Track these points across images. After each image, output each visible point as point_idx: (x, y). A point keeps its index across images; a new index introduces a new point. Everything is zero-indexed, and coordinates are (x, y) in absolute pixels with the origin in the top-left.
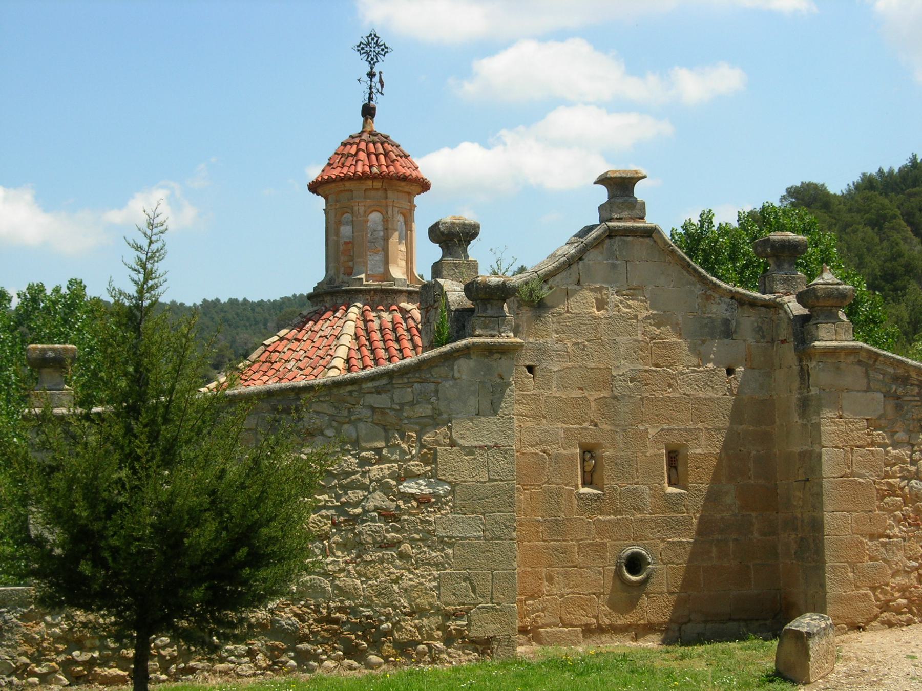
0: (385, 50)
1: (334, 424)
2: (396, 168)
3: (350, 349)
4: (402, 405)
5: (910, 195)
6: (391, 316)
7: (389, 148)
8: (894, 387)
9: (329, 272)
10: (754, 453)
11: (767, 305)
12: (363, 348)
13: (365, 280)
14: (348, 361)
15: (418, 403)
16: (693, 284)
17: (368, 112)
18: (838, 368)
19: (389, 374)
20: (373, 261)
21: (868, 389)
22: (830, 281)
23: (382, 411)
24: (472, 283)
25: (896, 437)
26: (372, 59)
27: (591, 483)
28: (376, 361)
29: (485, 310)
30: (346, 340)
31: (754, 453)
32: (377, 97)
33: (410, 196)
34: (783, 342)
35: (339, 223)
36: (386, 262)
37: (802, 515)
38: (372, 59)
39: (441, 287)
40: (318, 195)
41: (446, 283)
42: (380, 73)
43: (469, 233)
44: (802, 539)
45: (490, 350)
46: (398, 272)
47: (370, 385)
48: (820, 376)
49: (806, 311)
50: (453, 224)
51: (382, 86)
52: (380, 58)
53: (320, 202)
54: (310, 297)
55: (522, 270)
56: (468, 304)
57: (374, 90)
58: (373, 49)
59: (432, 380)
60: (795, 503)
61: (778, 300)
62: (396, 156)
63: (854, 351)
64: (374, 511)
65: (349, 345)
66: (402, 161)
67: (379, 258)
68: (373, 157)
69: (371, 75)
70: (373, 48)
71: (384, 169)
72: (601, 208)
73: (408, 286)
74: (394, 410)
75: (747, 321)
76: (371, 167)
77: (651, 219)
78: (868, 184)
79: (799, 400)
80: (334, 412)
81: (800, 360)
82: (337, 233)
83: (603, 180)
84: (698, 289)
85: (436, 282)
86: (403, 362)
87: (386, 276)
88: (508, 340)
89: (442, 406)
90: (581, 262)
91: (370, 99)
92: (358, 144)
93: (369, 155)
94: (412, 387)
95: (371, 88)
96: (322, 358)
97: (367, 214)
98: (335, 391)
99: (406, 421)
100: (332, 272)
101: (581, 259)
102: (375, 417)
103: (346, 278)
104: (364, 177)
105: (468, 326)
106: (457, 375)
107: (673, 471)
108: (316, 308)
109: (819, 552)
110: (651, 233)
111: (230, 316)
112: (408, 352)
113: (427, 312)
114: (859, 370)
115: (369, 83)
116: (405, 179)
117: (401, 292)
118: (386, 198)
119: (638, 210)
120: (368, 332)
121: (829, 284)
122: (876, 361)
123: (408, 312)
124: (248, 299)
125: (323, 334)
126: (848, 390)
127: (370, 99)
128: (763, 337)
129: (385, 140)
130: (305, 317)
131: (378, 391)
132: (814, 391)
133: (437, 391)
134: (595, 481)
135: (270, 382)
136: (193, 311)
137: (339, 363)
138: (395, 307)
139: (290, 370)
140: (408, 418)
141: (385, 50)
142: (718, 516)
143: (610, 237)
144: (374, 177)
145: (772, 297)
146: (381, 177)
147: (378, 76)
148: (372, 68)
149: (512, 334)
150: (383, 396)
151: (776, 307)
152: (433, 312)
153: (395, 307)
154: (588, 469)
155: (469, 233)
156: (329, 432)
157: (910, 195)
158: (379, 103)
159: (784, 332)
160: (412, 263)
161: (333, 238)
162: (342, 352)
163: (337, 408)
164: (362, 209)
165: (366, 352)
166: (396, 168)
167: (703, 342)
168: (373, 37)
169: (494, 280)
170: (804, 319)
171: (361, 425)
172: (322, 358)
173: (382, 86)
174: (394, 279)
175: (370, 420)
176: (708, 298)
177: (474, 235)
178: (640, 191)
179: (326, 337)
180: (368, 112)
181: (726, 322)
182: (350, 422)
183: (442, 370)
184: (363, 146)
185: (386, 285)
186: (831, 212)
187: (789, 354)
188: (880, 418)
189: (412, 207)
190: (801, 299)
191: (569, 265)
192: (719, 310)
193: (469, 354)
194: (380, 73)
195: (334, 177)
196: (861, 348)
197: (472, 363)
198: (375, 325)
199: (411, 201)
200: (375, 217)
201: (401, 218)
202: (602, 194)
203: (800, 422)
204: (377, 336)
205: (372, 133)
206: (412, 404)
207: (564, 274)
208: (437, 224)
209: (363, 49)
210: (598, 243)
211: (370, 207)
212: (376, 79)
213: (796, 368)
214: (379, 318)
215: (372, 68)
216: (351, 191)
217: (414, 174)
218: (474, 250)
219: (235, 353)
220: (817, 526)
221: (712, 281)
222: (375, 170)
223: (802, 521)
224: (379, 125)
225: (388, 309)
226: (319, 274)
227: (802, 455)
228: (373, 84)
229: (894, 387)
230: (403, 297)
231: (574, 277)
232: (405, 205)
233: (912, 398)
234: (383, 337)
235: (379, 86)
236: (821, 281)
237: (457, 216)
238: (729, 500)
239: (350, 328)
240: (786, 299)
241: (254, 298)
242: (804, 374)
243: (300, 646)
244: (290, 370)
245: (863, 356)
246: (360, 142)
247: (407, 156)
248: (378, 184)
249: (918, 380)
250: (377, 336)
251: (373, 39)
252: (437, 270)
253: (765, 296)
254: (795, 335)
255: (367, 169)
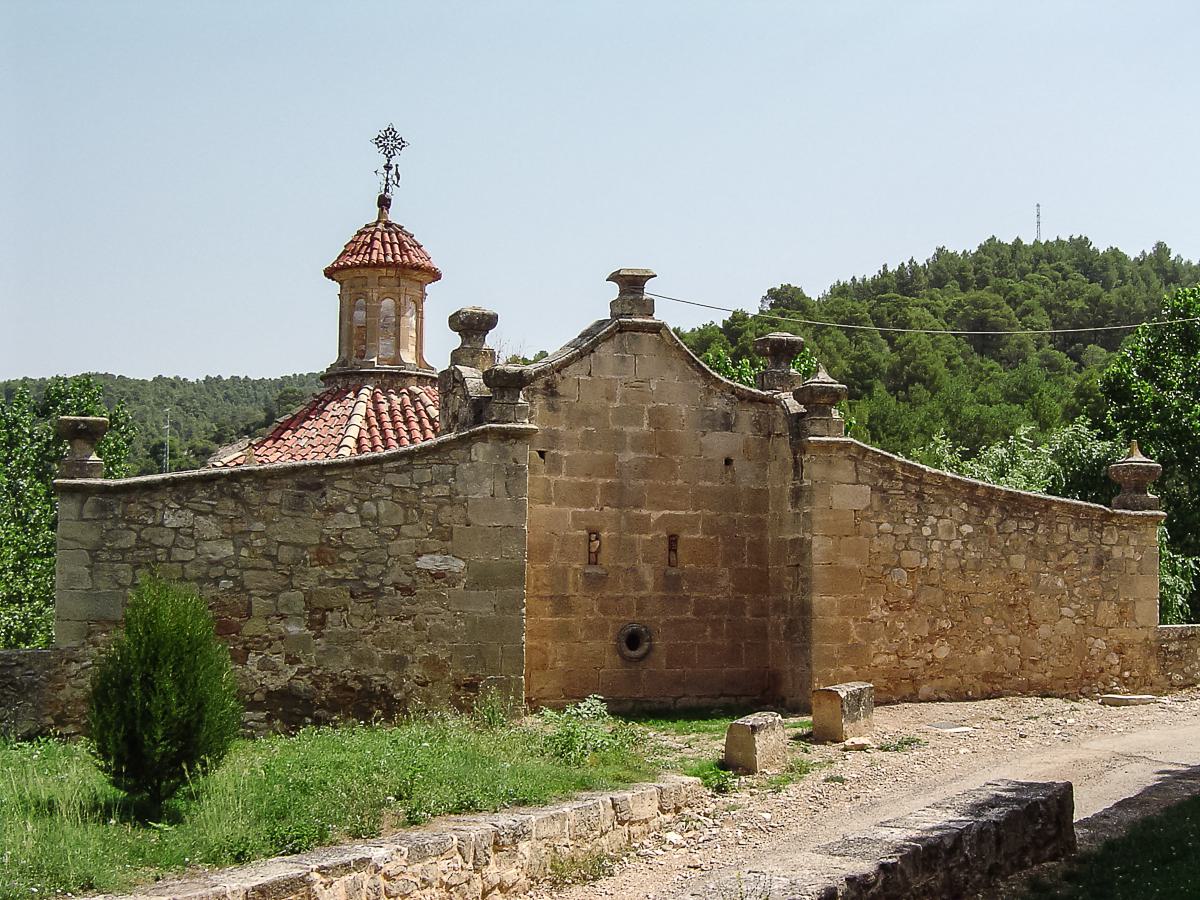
0: (402, 144)
1: (356, 501)
2: (409, 258)
3: (361, 429)
4: (421, 485)
5: (881, 300)
6: (400, 399)
7: (404, 238)
8: (881, 481)
9: (342, 355)
10: (748, 539)
11: (764, 400)
12: (374, 428)
13: (376, 362)
14: (358, 440)
15: (437, 483)
16: (697, 378)
17: (384, 203)
18: (830, 462)
19: (409, 455)
20: (384, 346)
21: (857, 483)
22: (825, 381)
23: (402, 490)
24: (490, 371)
25: (881, 527)
26: (389, 152)
27: (596, 564)
28: (412, 441)
29: (502, 397)
30: (357, 420)
31: (748, 539)
32: (393, 189)
33: (422, 285)
34: (778, 435)
35: (353, 308)
36: (398, 347)
37: (792, 599)
38: (389, 152)
39: (460, 373)
40: (333, 280)
41: (465, 371)
42: (397, 165)
43: (487, 322)
44: (791, 621)
45: (507, 435)
46: (408, 356)
47: (391, 465)
48: (814, 470)
49: (801, 409)
50: (473, 313)
51: (398, 178)
52: (397, 151)
53: (335, 287)
54: (324, 378)
55: (543, 354)
56: (486, 391)
57: (390, 182)
58: (390, 143)
59: (451, 462)
60: (786, 587)
61: (775, 396)
62: (410, 246)
63: (846, 446)
64: (391, 585)
65: (360, 425)
66: (416, 251)
67: (390, 343)
68: (388, 246)
69: (388, 167)
70: (390, 142)
71: (398, 258)
72: (613, 304)
73: (417, 370)
74: (415, 489)
75: (747, 415)
76: (385, 255)
77: (659, 316)
78: (840, 291)
79: (792, 490)
80: (357, 490)
81: (795, 454)
82: (351, 318)
83: (615, 277)
84: (700, 384)
85: (455, 368)
86: (424, 444)
87: (397, 360)
88: (523, 426)
89: (459, 487)
90: (592, 354)
91: (386, 190)
92: (373, 233)
93: (384, 244)
94: (430, 468)
95: (387, 180)
96: (333, 437)
97: (380, 299)
98: (357, 469)
99: (424, 500)
100: (345, 355)
101: (593, 351)
102: (395, 496)
103: (358, 361)
104: (379, 265)
105: (485, 413)
106: (474, 458)
107: (673, 555)
108: (328, 389)
109: (807, 633)
110: (658, 328)
111: (230, 393)
112: (430, 434)
113: (445, 397)
114: (850, 465)
115: (386, 175)
116: (418, 268)
117: (410, 375)
118: (399, 286)
119: (648, 307)
120: (378, 413)
121: (824, 383)
122: (864, 456)
123: (417, 395)
124: (210, 375)
125: (335, 414)
126: (839, 483)
127: (386, 190)
128: (760, 431)
129: (399, 230)
130: (317, 397)
131: (399, 470)
132: (807, 483)
133: (454, 472)
134: (599, 562)
135: (283, 459)
136: (196, 387)
137: (351, 442)
138: (404, 390)
139: (303, 448)
140: (426, 497)
141: (402, 144)
142: (714, 598)
143: (620, 331)
144: (387, 265)
145: (769, 393)
146: (395, 265)
147: (394, 168)
148: (389, 161)
149: (527, 421)
150: (404, 475)
151: (775, 402)
152: (451, 397)
153: (404, 390)
154: (593, 550)
155: (487, 322)
156: (351, 509)
157: (881, 300)
158: (395, 195)
159: (781, 426)
160: (422, 348)
161: (346, 322)
162: (353, 431)
163: (359, 486)
164: (375, 295)
165: (376, 432)
166: (409, 258)
167: (704, 433)
168: (391, 131)
169: (512, 368)
170: (800, 416)
171: (382, 503)
172: (333, 437)
173: (398, 178)
174: (405, 364)
175: (390, 498)
176: (710, 392)
177: (493, 325)
178: (650, 289)
179: (337, 416)
180: (384, 203)
181: (726, 415)
182: (371, 500)
183: (461, 453)
184: (378, 235)
185: (395, 369)
186: (807, 314)
187: (784, 448)
188: (867, 509)
189: (423, 296)
190: (797, 396)
191: (582, 357)
192: (718, 404)
193: (487, 438)
194: (397, 165)
195: (350, 263)
196: (852, 442)
197: (488, 447)
198: (384, 407)
199: (422, 290)
200: (388, 303)
201: (413, 306)
202: (614, 290)
203: (792, 511)
204: (386, 418)
205: (388, 225)
206: (431, 484)
207: (577, 365)
208: (457, 313)
209: (381, 142)
210: (610, 336)
211: (384, 293)
212: (392, 172)
213: (790, 460)
214: (389, 400)
215: (389, 161)
216: (366, 277)
217: (427, 264)
218: (491, 340)
219: (236, 428)
220: (805, 609)
221: (714, 377)
222: (390, 259)
223: (792, 603)
224: (393, 216)
225: (399, 394)
226: (333, 357)
227: (794, 541)
228: (389, 177)
229: (881, 481)
230: (413, 380)
231: (586, 368)
232: (417, 293)
233: (895, 492)
234: (391, 418)
235: (395, 178)
236: (816, 380)
237: (477, 306)
238: (723, 583)
239: (361, 409)
240: (783, 395)
241: (255, 377)
242: (797, 467)
243: (55, 481)
244: (303, 448)
245: (853, 452)
246: (375, 232)
247: (420, 247)
248: (391, 272)
249: (903, 475)
250: (386, 418)
251: (391, 133)
252: (456, 357)
253: (765, 393)
254: (790, 429)
255: (382, 257)
